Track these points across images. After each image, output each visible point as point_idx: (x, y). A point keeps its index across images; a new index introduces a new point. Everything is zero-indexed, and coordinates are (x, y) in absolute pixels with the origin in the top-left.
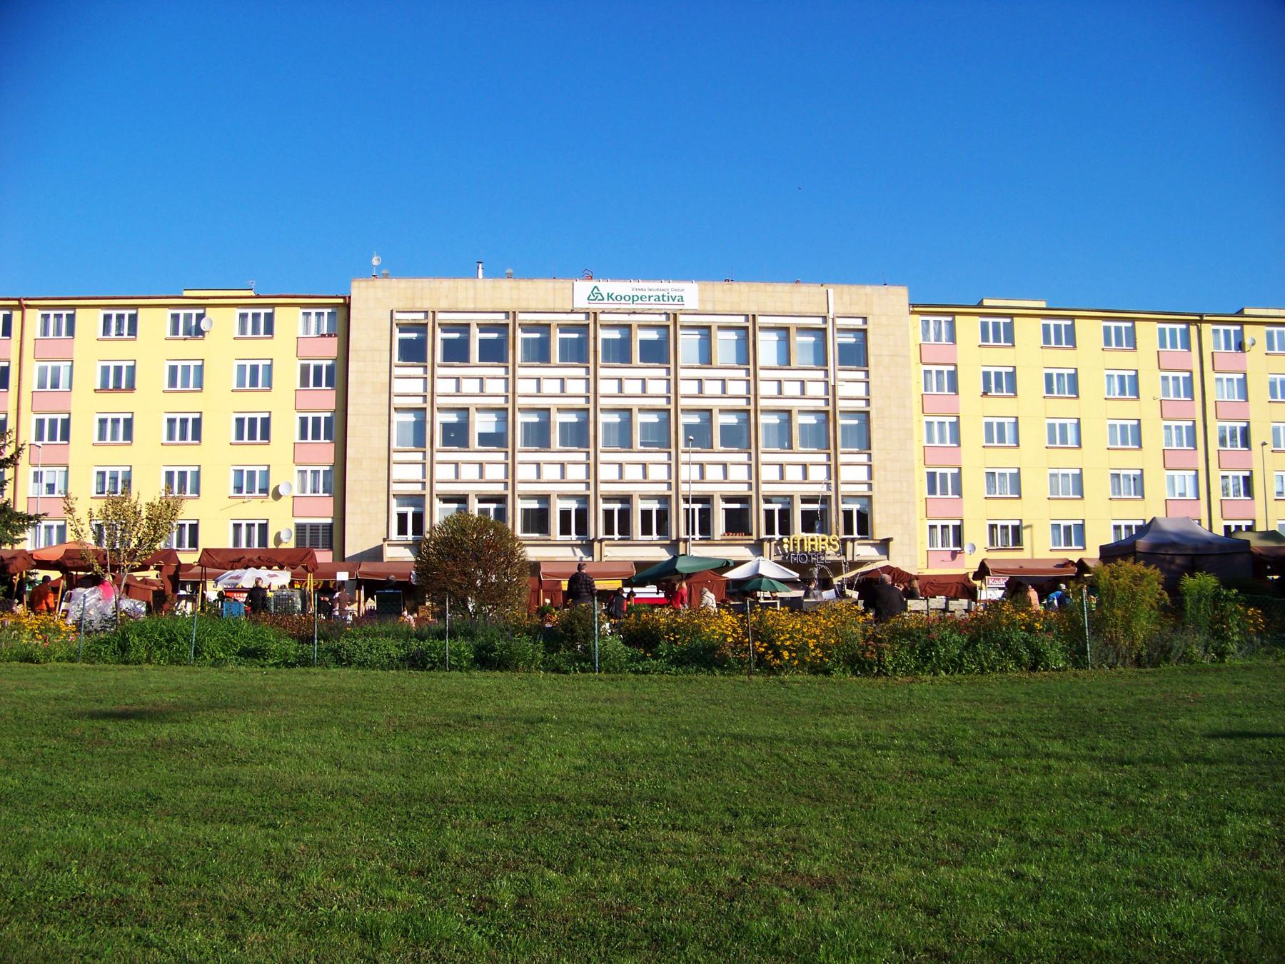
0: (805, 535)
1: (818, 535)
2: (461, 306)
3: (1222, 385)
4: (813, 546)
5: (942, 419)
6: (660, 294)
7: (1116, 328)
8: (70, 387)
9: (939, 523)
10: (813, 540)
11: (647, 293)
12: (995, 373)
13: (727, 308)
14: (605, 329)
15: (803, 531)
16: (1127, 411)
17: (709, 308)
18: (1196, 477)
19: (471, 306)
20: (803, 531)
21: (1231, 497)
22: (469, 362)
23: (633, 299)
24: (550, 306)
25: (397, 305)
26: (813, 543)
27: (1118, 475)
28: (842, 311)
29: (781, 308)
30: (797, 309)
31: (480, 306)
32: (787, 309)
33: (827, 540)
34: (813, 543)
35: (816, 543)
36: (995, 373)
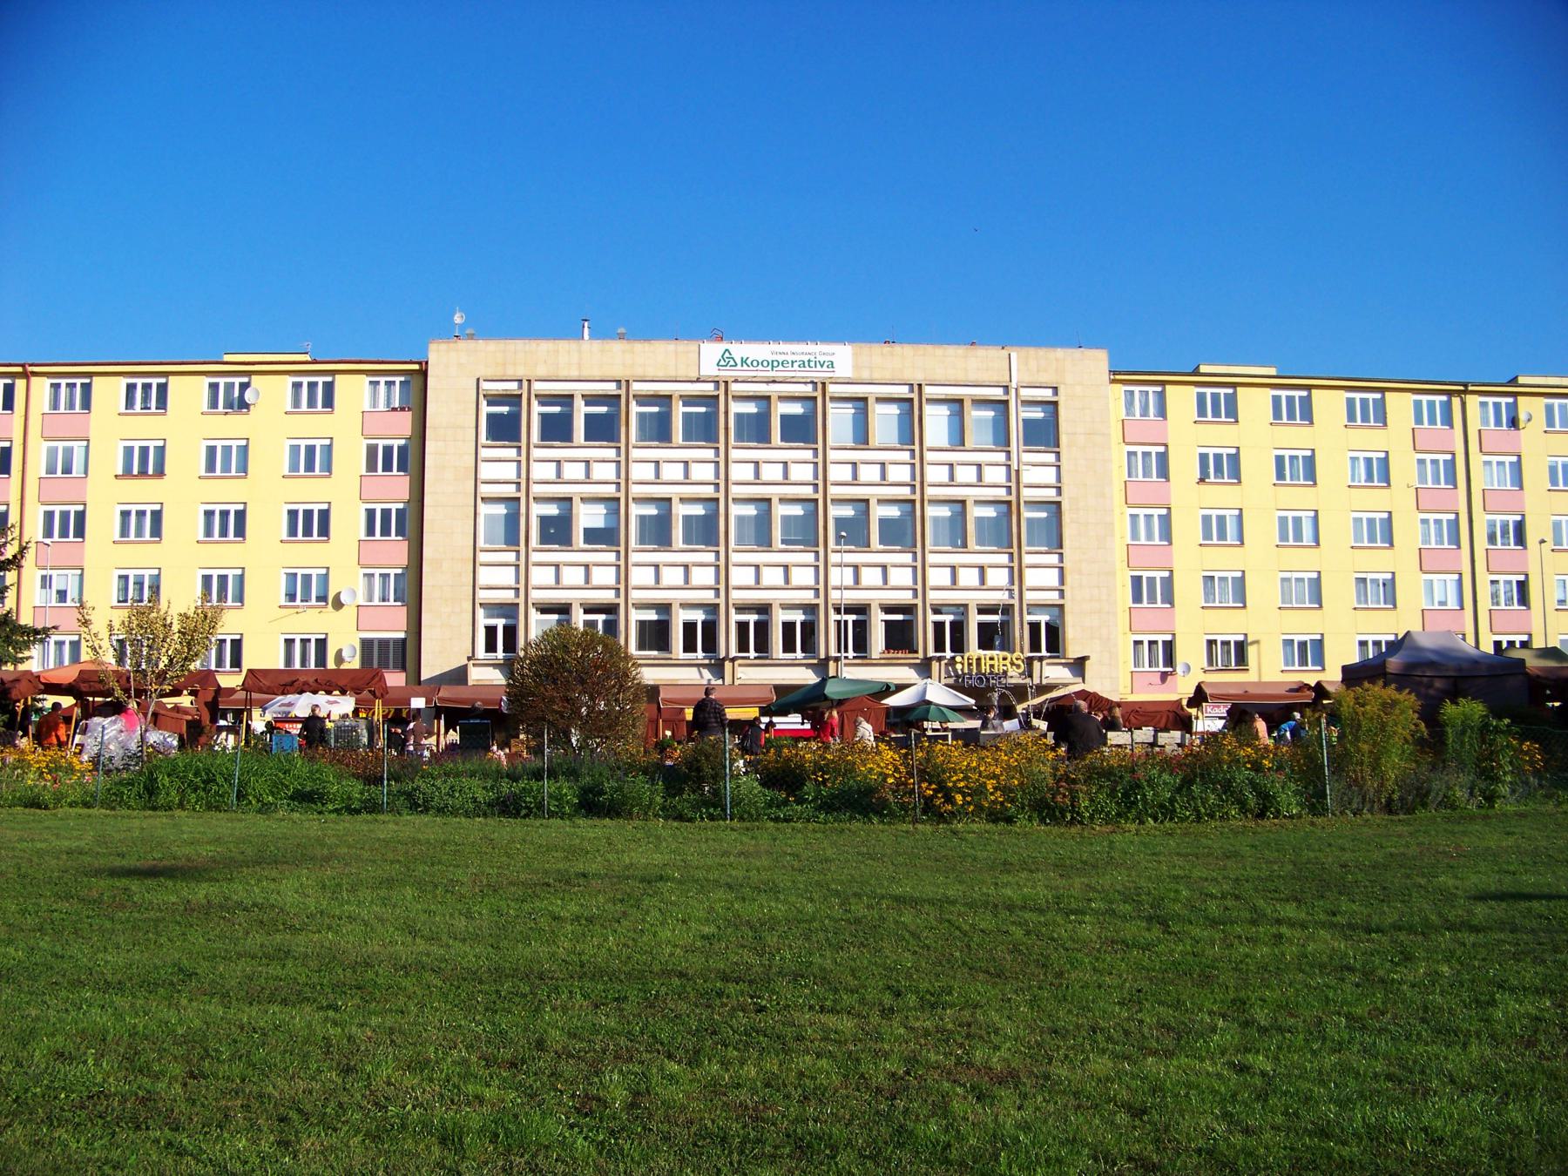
0: (982, 652)
1: (998, 652)
2: (563, 374)
5: (1149, 511)
6: (806, 358)
9: (1146, 638)
10: (992, 659)
11: (790, 358)
12: (1214, 455)
13: (887, 376)
15: (979, 648)
17: (865, 375)
18: (1460, 582)
19: (574, 374)
20: (979, 648)
22: (572, 442)
23: (772, 365)
24: (672, 373)
25: (484, 372)
26: (992, 662)
27: (1364, 580)
28: (1027, 379)
29: (952, 375)
30: (973, 377)
31: (586, 374)
32: (960, 376)
33: (1009, 659)
34: (992, 662)
35: (995, 662)
36: (1214, 455)
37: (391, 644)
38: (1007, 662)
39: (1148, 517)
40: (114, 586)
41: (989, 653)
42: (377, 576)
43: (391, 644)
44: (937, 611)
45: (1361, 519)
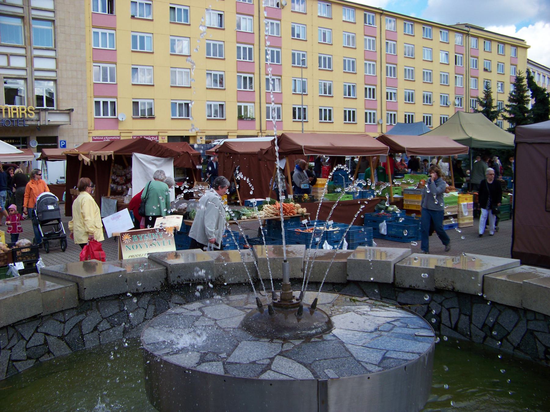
0: (9, 106)
1: (18, 106)
3: (28, 205)
4: (15, 114)
7: (277, 52)
8: (548, 211)
9: (101, 100)
10: (15, 109)
12: (249, 48)
14: (224, 113)
15: (6, 104)
16: (217, 97)
20: (6, 104)
21: (102, 116)
26: (15, 112)
27: (174, 8)
33: (25, 110)
34: (15, 112)
35: (17, 112)
36: (249, 48)
37: (456, 182)
38: (25, 112)
39: (245, 49)
40: (192, 112)
41: (12, 106)
42: (242, 58)
43: (456, 182)
44: (471, 97)
45: (246, 48)
